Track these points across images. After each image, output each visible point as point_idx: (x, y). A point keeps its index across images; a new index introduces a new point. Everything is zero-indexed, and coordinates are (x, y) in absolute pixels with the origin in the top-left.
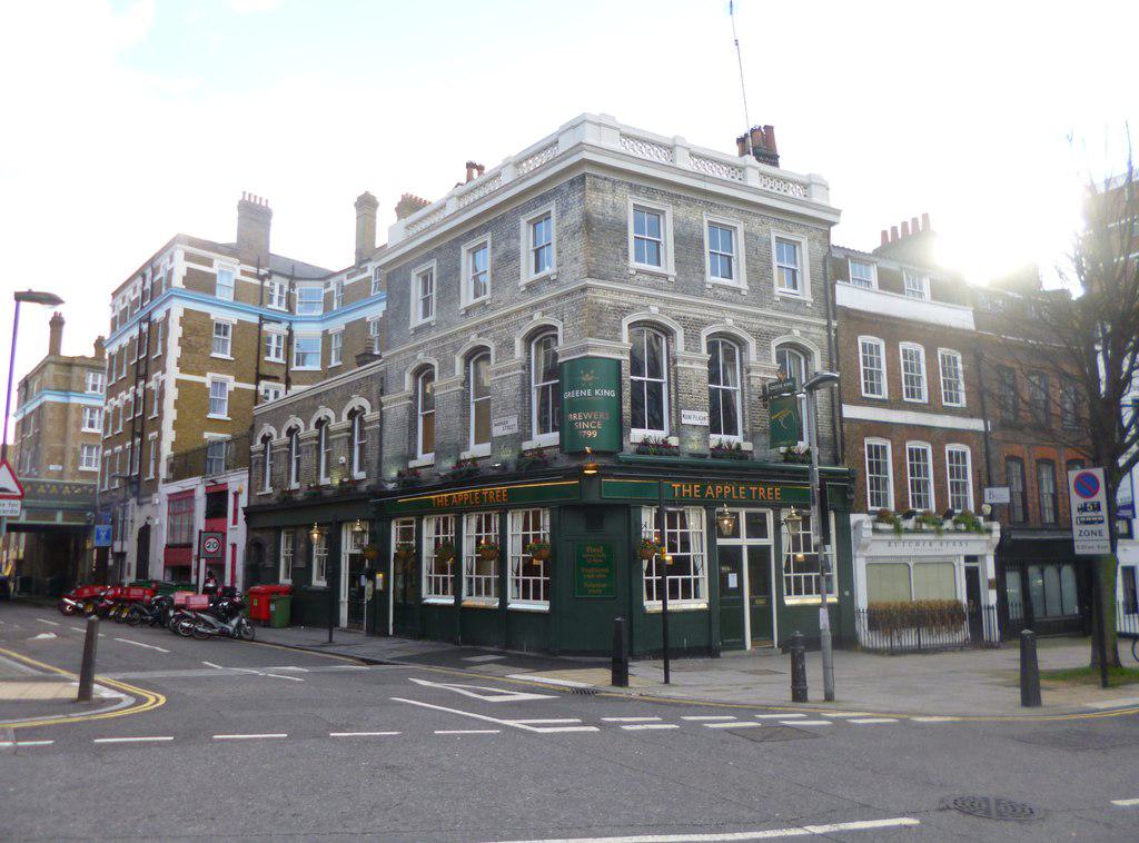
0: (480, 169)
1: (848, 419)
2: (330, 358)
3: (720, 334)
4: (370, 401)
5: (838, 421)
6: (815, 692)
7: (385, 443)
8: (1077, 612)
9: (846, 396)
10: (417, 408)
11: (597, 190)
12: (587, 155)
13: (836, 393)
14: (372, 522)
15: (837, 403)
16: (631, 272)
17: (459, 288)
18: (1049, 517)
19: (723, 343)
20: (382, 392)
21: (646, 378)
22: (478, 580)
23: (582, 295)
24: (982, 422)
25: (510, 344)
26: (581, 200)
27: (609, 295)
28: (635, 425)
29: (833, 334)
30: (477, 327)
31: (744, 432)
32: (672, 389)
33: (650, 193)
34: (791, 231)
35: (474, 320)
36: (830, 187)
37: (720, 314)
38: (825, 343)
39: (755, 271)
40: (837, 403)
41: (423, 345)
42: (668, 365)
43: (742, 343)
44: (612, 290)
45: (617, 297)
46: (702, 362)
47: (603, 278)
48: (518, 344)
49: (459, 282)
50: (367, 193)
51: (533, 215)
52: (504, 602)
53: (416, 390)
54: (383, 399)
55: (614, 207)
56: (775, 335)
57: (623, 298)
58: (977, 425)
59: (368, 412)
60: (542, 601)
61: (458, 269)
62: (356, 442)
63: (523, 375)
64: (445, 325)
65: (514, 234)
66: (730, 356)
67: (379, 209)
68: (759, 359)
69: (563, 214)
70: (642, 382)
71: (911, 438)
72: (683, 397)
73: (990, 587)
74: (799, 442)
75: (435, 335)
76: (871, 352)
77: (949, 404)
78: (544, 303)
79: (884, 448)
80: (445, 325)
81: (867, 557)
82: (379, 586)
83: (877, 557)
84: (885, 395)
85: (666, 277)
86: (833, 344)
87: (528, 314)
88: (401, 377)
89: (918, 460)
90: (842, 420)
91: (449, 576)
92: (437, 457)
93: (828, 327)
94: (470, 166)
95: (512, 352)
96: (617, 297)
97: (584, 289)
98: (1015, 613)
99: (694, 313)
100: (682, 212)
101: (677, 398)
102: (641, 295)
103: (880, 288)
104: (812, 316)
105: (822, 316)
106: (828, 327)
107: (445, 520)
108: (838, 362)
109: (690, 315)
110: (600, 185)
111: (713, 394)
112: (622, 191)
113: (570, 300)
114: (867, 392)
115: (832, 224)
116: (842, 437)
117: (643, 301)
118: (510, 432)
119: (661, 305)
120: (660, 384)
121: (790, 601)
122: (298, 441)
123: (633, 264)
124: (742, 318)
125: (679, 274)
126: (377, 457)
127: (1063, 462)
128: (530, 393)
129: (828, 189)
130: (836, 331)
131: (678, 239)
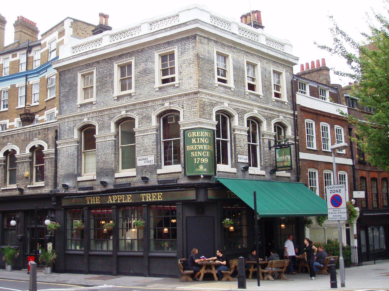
5: (298, 160)
6: (339, 284)
8: (385, 248)
10: (81, 148)
11: (201, 43)
18: (375, 205)
19: (251, 121)
21: (221, 139)
24: (351, 160)
25: (149, 118)
27: (207, 97)
32: (233, 145)
33: (223, 45)
34: (278, 67)
43: (231, 116)
44: (209, 94)
45: (211, 98)
47: (205, 88)
49: (112, 82)
51: (164, 51)
54: (58, 142)
55: (209, 53)
56: (273, 118)
58: (349, 162)
59: (46, 149)
62: (34, 165)
70: (220, 140)
71: (310, 167)
73: (355, 238)
74: (36, 147)
75: (94, 108)
77: (309, 148)
87: (160, 102)
89: (342, 180)
90: (300, 160)
96: (211, 98)
98: (364, 250)
99: (241, 106)
101: (235, 149)
106: (294, 115)
110: (203, 41)
112: (212, 44)
113: (187, 97)
117: (222, 100)
118: (149, 164)
119: (228, 102)
120: (226, 142)
127: (380, 179)
128: (160, 144)
129: (292, 47)
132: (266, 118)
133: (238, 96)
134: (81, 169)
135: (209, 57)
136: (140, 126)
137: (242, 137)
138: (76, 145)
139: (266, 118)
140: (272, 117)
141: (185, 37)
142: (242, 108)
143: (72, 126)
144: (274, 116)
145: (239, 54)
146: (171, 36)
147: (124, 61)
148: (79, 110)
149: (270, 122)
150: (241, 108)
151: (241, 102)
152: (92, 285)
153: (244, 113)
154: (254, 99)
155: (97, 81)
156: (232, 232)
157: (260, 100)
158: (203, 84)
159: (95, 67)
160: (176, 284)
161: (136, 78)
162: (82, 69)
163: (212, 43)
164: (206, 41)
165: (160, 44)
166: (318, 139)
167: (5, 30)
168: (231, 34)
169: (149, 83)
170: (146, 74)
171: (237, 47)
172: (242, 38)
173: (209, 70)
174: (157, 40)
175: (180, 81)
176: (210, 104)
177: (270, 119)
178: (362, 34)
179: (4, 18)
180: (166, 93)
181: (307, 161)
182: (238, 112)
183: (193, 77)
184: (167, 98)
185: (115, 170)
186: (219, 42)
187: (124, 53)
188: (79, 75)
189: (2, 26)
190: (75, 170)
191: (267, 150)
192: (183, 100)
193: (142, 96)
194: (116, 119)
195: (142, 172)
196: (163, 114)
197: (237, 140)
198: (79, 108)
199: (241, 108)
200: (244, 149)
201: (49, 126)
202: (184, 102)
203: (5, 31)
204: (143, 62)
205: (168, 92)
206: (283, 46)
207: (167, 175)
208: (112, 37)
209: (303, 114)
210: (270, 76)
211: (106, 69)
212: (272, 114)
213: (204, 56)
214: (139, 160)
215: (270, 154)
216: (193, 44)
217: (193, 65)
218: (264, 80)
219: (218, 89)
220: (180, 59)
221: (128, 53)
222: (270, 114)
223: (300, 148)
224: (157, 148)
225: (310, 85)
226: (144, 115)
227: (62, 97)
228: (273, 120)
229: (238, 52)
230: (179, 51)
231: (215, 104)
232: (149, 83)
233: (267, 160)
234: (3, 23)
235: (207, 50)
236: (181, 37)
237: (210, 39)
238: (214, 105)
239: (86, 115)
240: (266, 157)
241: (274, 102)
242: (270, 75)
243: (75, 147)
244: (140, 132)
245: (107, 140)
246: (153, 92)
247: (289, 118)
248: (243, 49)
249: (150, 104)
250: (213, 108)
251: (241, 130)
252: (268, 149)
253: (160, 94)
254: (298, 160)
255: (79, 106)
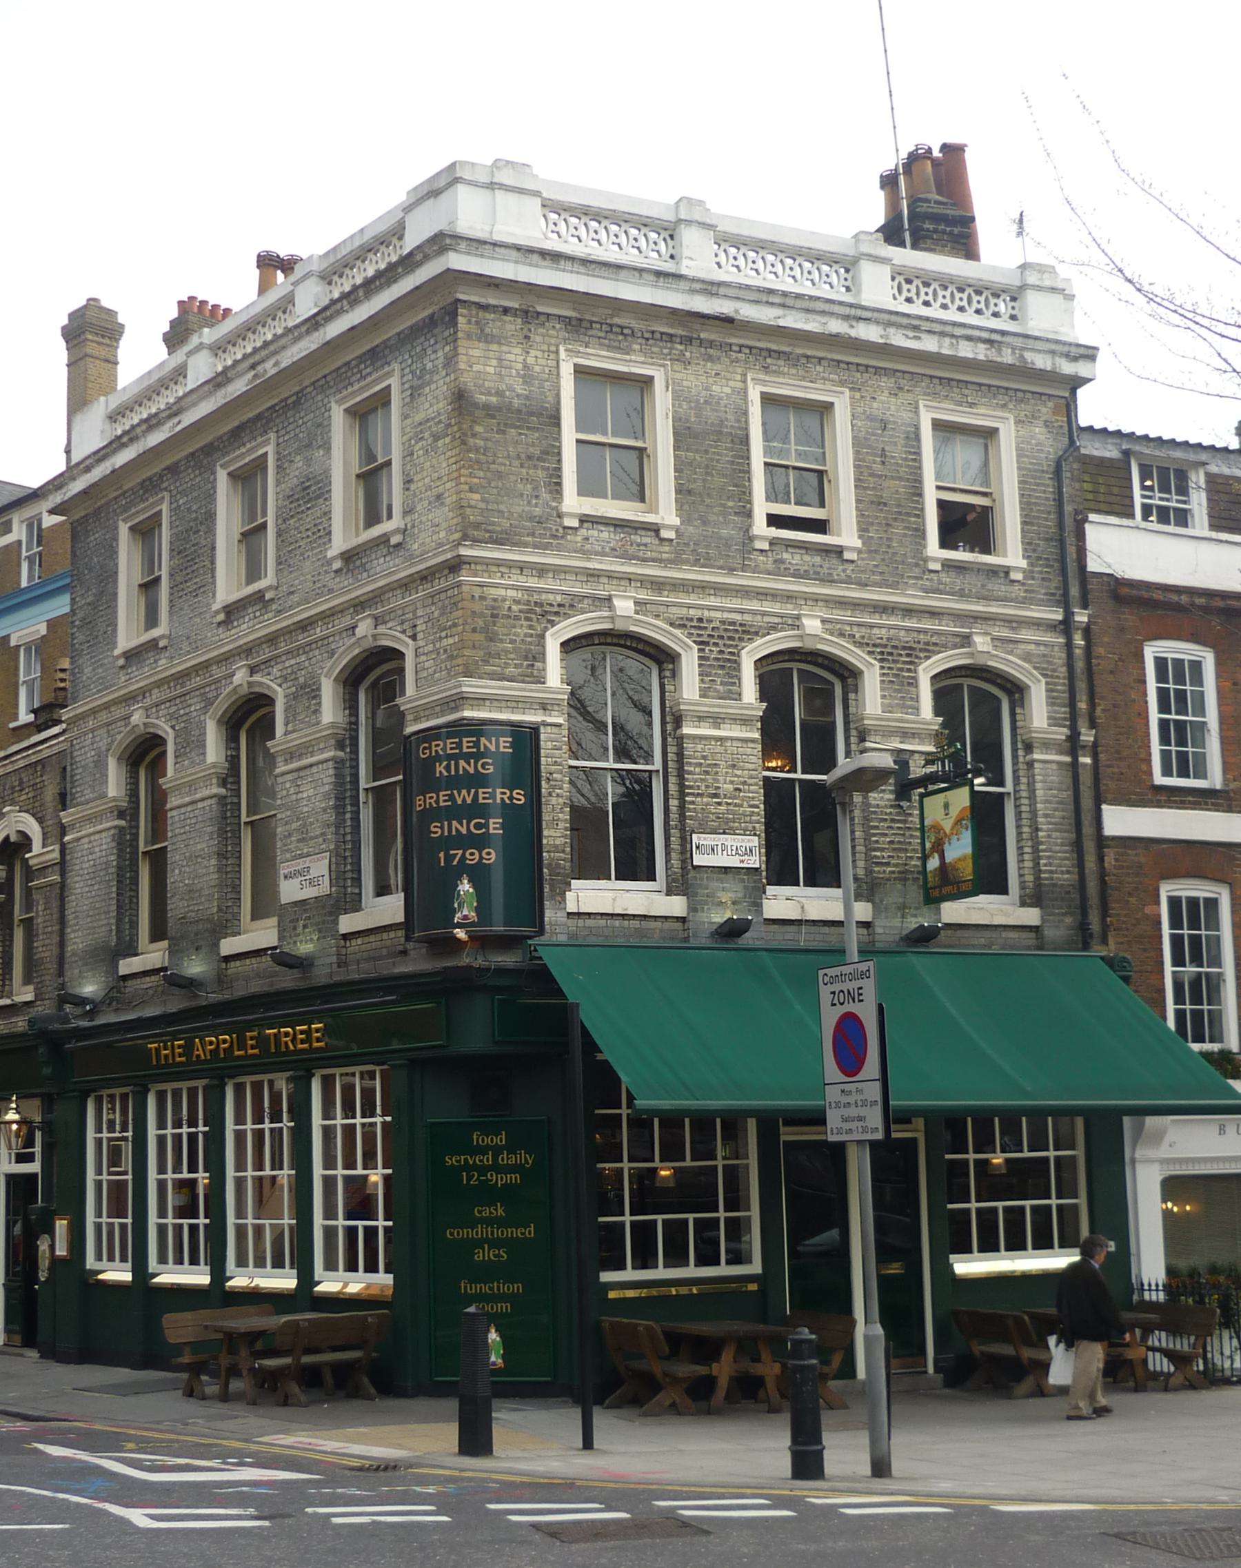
0: (287, 265)
1: (1114, 838)
2: (16, 706)
3: (791, 654)
4: (40, 821)
7: (70, 917)
9: (1112, 785)
10: (136, 836)
11: (487, 338)
12: (458, 261)
13: (1086, 778)
14: (48, 1103)
15: (1087, 802)
16: (568, 522)
17: (213, 562)
20: (63, 800)
22: (351, 1233)
23: (451, 580)
25: (311, 692)
26: (451, 361)
27: (516, 579)
28: (590, 868)
29: (1079, 641)
30: (247, 651)
31: (856, 879)
32: (672, 788)
34: (971, 405)
35: (140, 677)
36: (1076, 290)
37: (789, 609)
38: (1059, 657)
39: (880, 503)
40: (1087, 802)
41: (143, 692)
42: (664, 731)
44: (522, 567)
45: (533, 583)
46: (745, 721)
47: (498, 540)
48: (329, 693)
50: (92, 303)
51: (359, 394)
52: (219, 1274)
53: (133, 794)
54: (66, 817)
57: (549, 583)
59: (37, 847)
60: (287, 1270)
61: (211, 517)
63: (222, 800)
64: (185, 646)
65: (319, 438)
66: (820, 698)
67: (123, 343)
68: (887, 709)
69: (414, 393)
72: (696, 804)
75: (164, 666)
76: (1180, 679)
78: (377, 597)
79: (1212, 904)
80: (185, 646)
81: (1164, 1162)
82: (61, 1251)
83: (1193, 1160)
84: (1215, 778)
85: (655, 529)
86: (1080, 665)
88: (100, 764)
90: (1102, 841)
91: (381, 1223)
92: (173, 951)
93: (1066, 626)
94: (269, 263)
95: (317, 712)
96: (533, 583)
97: (455, 566)
99: (718, 608)
100: (695, 378)
101: (682, 807)
102: (593, 575)
103: (1214, 527)
104: (1025, 602)
105: (1051, 601)
106: (1066, 626)
107: (193, 1093)
108: (1092, 705)
109: (713, 614)
111: (776, 793)
114: (1167, 772)
115: (1081, 381)
116: (1103, 883)
121: (967, 1266)
122: (29, 873)
123: (572, 502)
124: (846, 616)
125: (686, 520)
126: (56, 951)
128: (356, 803)
130: (1087, 632)
131: (683, 436)
132: (882, 653)
133: (701, 561)
134: (134, 925)
135: (527, 398)
136: (290, 727)
137: (721, 749)
138: (115, 827)
139: (882, 653)
140: (921, 646)
141: (423, 320)
142: (726, 615)
143: (103, 745)
144: (934, 640)
145: (718, 367)
146: (374, 322)
147: (243, 456)
148: (123, 679)
149: (909, 670)
150: (718, 615)
151: (718, 589)
152: (36, 1414)
153: (741, 639)
154: (806, 568)
155: (172, 550)
156: (666, 1190)
157: (844, 571)
158: (493, 524)
159: (166, 489)
160: (365, 1425)
161: (280, 521)
162: (132, 504)
163: (552, 332)
164: (512, 325)
165: (347, 364)
166: (1230, 733)
167: (116, 363)
168: (652, 278)
169: (315, 541)
170: (308, 502)
171: (702, 335)
172: (722, 291)
173: (529, 458)
174: (331, 346)
175: (408, 519)
176: (530, 611)
177: (908, 655)
178: (1021, 215)
179: (112, 314)
180: (365, 575)
181: (1156, 847)
182: (699, 635)
183: (446, 495)
184: (366, 597)
185: (226, 925)
186: (592, 322)
187: (245, 418)
188: (124, 530)
189: (103, 352)
190: (111, 930)
191: (882, 803)
192: (414, 602)
193: (295, 598)
194: (221, 705)
195: (295, 928)
196: (820, 660)
197: (690, 764)
198: (122, 667)
199: (718, 615)
200: (736, 805)
201: (45, 754)
202: (419, 613)
203: (119, 367)
204: (298, 451)
205: (372, 572)
206: (1014, 299)
207: (372, 938)
208: (220, 353)
209: (1130, 618)
210: (915, 453)
211: (195, 494)
212: (919, 631)
213: (499, 393)
214: (286, 877)
215: (905, 822)
216: (447, 349)
217: (447, 440)
218: (871, 475)
219: (579, 539)
220: (409, 421)
221: (259, 417)
222: (908, 630)
223: (1108, 784)
224: (339, 824)
225: (1213, 469)
226: (302, 680)
227: (79, 627)
228: (928, 658)
229: (710, 358)
230: (407, 386)
231: (562, 610)
232: (315, 541)
233: (883, 850)
234: (103, 336)
235: (520, 366)
236: (409, 323)
237: (539, 313)
238: (557, 613)
239: (140, 698)
240: (874, 835)
241: (937, 572)
242: (913, 447)
243: (112, 832)
244: (291, 755)
245: (198, 796)
246: (328, 577)
247: (1037, 644)
248: (742, 341)
249: (318, 630)
250: (546, 629)
251: (717, 720)
252: (892, 797)
253: (346, 583)
254: (1089, 846)
255: (121, 662)
